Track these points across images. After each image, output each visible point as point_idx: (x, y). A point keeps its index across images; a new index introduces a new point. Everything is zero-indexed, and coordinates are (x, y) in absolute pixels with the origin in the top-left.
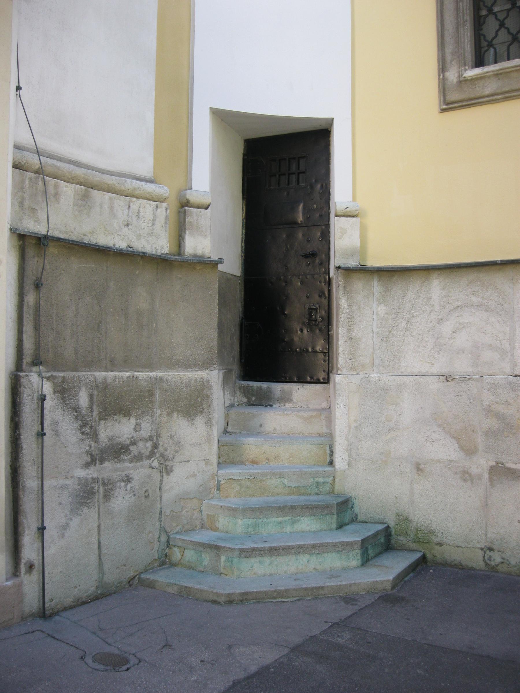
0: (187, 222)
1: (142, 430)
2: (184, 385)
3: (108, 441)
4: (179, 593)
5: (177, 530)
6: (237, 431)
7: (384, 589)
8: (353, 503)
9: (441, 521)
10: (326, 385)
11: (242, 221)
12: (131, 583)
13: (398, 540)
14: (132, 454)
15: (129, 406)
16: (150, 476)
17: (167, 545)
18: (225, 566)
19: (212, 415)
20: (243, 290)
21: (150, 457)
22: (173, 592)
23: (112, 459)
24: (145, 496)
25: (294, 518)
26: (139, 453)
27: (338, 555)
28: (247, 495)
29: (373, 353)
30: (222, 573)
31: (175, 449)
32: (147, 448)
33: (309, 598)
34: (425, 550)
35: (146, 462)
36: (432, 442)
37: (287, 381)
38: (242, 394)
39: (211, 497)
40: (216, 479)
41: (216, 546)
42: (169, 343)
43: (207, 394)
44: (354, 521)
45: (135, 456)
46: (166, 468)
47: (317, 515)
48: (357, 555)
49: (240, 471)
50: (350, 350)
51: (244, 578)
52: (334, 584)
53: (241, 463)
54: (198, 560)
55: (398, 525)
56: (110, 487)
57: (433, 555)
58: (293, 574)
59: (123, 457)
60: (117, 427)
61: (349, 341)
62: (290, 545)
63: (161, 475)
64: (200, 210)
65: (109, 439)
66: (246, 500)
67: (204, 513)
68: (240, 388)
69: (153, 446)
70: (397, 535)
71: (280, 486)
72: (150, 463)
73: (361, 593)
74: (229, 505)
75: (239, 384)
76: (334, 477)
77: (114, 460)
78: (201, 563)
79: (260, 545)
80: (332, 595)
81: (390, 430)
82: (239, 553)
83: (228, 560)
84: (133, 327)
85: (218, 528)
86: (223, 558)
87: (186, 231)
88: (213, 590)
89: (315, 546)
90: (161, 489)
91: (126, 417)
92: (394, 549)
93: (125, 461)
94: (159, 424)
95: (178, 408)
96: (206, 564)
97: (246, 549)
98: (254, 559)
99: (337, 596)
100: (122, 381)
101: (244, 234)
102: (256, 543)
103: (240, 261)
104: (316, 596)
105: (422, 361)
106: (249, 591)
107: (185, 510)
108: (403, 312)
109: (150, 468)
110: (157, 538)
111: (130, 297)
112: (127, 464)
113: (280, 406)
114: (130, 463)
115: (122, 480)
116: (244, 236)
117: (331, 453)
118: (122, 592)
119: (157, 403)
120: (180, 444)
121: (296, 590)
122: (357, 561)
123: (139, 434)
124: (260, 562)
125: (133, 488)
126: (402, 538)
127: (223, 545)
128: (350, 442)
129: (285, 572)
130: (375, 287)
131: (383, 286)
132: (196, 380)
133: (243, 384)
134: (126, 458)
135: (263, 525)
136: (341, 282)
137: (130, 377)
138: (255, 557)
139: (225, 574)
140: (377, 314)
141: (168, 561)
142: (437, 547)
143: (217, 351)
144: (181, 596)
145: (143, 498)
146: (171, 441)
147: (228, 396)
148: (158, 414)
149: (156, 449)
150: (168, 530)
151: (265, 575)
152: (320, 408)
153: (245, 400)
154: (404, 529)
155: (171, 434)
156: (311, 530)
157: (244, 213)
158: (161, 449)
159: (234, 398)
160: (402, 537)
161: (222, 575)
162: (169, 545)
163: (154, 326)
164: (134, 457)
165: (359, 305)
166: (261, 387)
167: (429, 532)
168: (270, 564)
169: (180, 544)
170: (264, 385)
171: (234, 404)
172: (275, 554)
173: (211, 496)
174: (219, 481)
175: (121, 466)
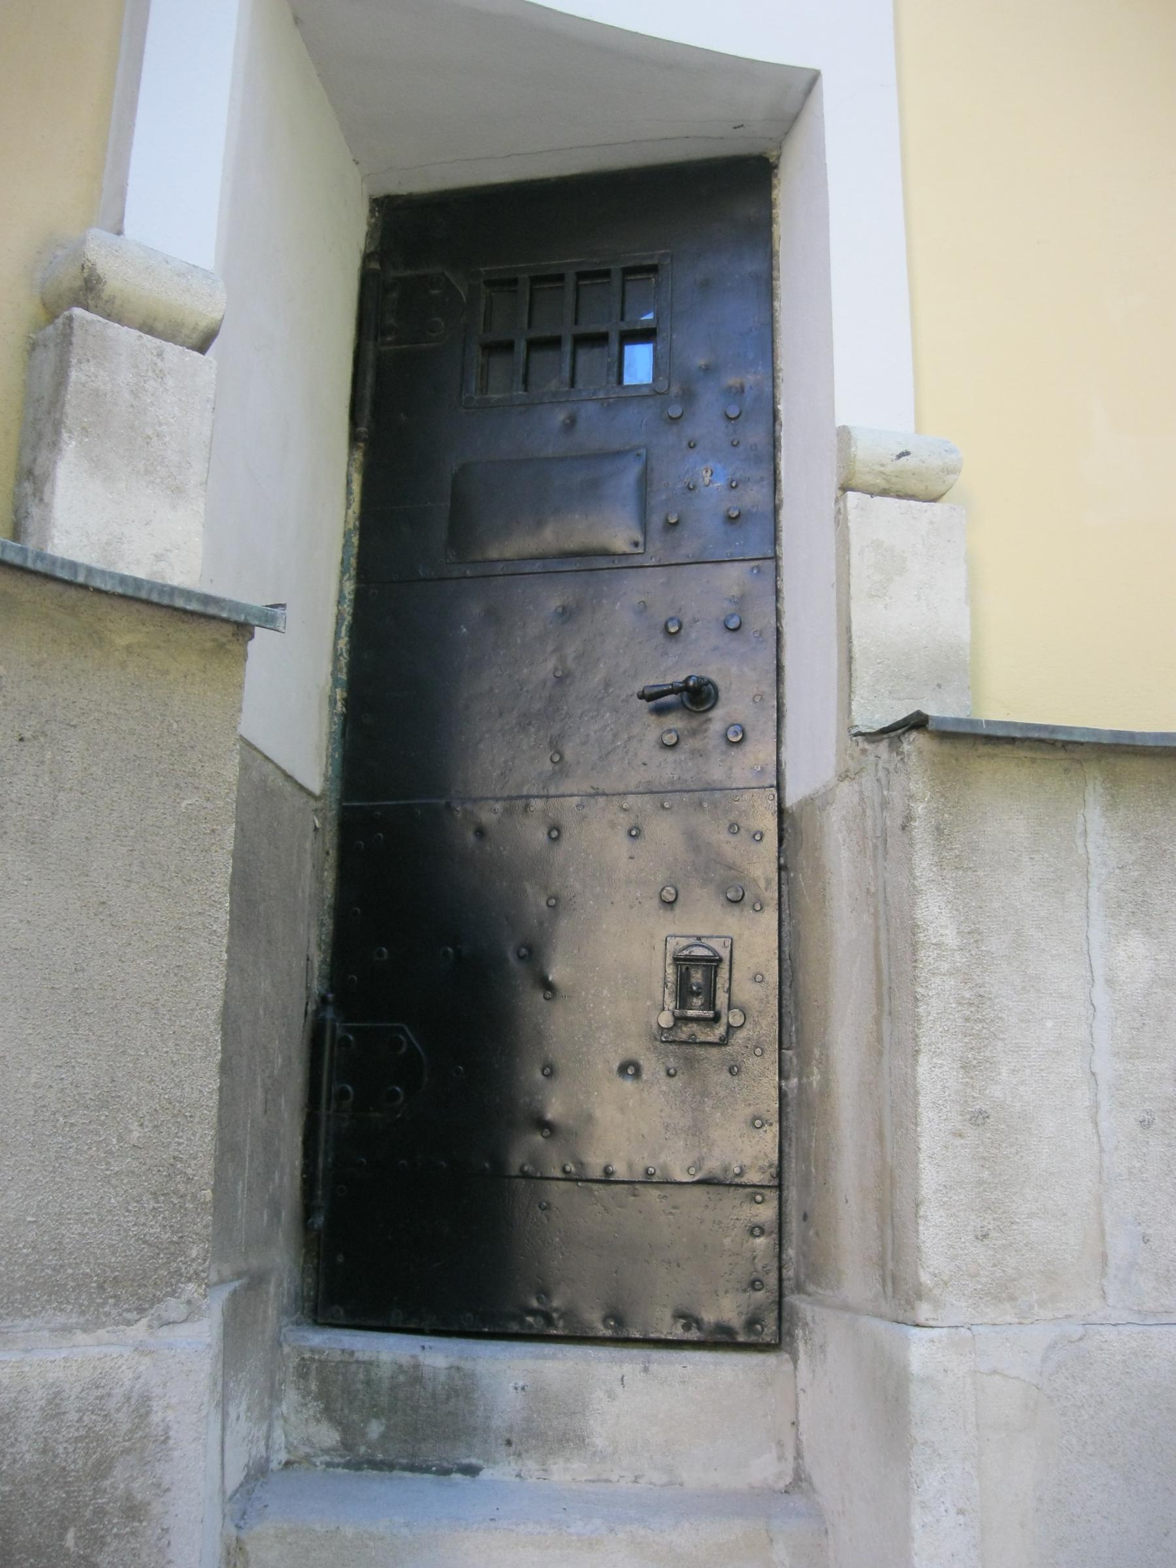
0: (71, 388)
11: (340, 541)
38: (315, 1407)
43: (129, 1496)
50: (981, 1182)
64: (158, 342)
68: (303, 1372)
87: (65, 435)
101: (349, 596)
103: (326, 722)
113: (519, 1475)
116: (347, 608)
133: (321, 1352)
136: (922, 800)
140: (1110, 982)
143: (214, 1191)
147: (241, 1427)
153: (328, 1436)
157: (356, 506)
166: (417, 1366)
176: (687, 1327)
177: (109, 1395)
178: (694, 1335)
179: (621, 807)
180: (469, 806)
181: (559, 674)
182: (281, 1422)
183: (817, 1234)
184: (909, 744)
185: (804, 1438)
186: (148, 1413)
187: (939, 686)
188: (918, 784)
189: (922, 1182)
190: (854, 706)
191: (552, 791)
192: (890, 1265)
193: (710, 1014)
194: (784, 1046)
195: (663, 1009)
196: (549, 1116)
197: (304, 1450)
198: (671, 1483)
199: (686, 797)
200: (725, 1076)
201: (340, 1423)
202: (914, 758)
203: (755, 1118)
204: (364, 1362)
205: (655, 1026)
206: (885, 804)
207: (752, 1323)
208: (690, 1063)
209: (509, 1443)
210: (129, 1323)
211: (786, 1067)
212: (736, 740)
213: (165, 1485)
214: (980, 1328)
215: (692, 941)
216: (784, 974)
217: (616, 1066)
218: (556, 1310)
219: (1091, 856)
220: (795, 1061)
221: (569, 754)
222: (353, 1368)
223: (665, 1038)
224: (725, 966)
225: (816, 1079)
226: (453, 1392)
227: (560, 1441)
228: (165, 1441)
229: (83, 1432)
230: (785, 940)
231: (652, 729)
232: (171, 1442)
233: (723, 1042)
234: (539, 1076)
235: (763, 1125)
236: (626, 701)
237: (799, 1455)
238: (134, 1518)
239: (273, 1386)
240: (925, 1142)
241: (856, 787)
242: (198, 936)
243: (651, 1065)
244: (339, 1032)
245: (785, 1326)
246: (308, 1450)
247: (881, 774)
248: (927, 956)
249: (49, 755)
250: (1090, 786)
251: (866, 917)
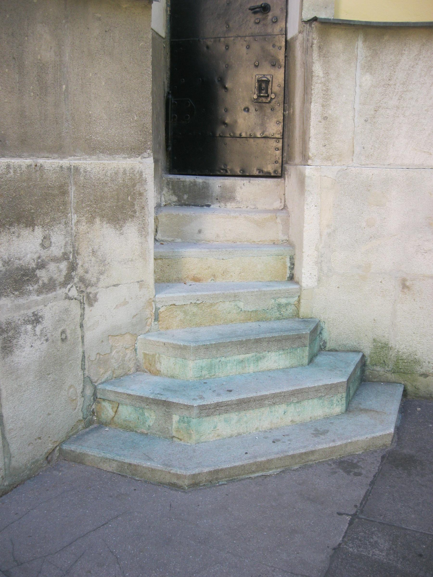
1: (53, 245)
2: (109, 179)
3: (4, 266)
4: (119, 472)
5: (106, 377)
6: (170, 239)
7: (384, 445)
8: (321, 328)
9: (428, 349)
10: (279, 180)
12: (49, 458)
13: (373, 370)
14: (41, 282)
15: (32, 211)
16: (67, 310)
17: (94, 399)
18: (178, 428)
19: (146, 221)
20: (168, 56)
21: (66, 284)
22: (110, 470)
23: (12, 293)
24: (62, 339)
25: (258, 355)
26: (51, 279)
27: (321, 401)
28: (193, 325)
29: (353, 139)
30: (174, 437)
31: (98, 270)
32: (61, 271)
33: (296, 467)
34: (405, 382)
35: (61, 292)
36: (424, 254)
37: (228, 174)
38: (171, 192)
39: (147, 330)
40: (154, 306)
41: (165, 401)
42: (86, 116)
43: (140, 191)
44: (322, 350)
45: (44, 284)
46: (88, 297)
47: (287, 348)
48: (342, 400)
49: (184, 294)
50: (325, 133)
51: (205, 442)
52: (327, 446)
53: (179, 280)
54: (138, 419)
55: (374, 353)
56: (10, 334)
57: (415, 388)
58: (266, 432)
59: (27, 287)
60: (16, 243)
61: (323, 121)
62: (263, 395)
63: (82, 307)
65: (5, 262)
66: (195, 332)
67: (140, 353)
68: (168, 184)
69: (68, 268)
70: (373, 365)
71: (235, 311)
72: (67, 291)
73: (357, 453)
74: (175, 342)
75: (167, 179)
76: (299, 296)
77: (13, 294)
78: (144, 423)
79: (225, 398)
80: (323, 460)
81: (371, 237)
82: (198, 411)
83: (182, 421)
84: (32, 88)
85: (160, 371)
86: (176, 418)
88: (171, 470)
89: (293, 393)
90: (83, 327)
91: (28, 228)
92: (369, 381)
93: (31, 293)
94: (76, 235)
95: (101, 211)
96: (151, 424)
97: (207, 405)
98: (217, 417)
99: (330, 460)
100: (19, 172)
102: (219, 395)
104: (304, 463)
105: (416, 150)
106: (220, 468)
107: (115, 351)
108: (395, 85)
109: (67, 299)
110: (80, 393)
111: (26, 38)
112: (34, 297)
113: (219, 207)
114: (38, 296)
115: (27, 322)
117: (292, 266)
118: (38, 475)
119: (72, 205)
120: (106, 262)
121: (281, 459)
122: (342, 407)
123: (49, 252)
124: (226, 421)
125: (45, 330)
126: (378, 368)
127: (175, 400)
128: (321, 253)
129: (257, 429)
130: (359, 49)
131: (370, 48)
132: (125, 171)
133: (172, 179)
134: (31, 288)
135: (221, 367)
137: (31, 165)
138: (219, 415)
139: (178, 438)
140: (360, 86)
141: (95, 418)
142: (421, 379)
144: (123, 476)
145: (59, 343)
146: (93, 259)
148: (74, 221)
149: (73, 271)
150: (94, 379)
151: (231, 437)
152: (271, 208)
153: (175, 198)
154: (381, 357)
155: (93, 249)
156: (278, 368)
158: (80, 271)
159: (161, 196)
160: (379, 367)
161: (175, 439)
162: (97, 398)
163: (64, 90)
164: (44, 286)
165: (338, 74)
166: (195, 182)
167: (412, 361)
168: (239, 421)
169: (112, 397)
170: (200, 180)
171: (161, 204)
172: (245, 408)
173: (148, 328)
174: (157, 309)
175: (25, 302)
176: (259, 172)
177: (135, 171)
178: (261, 174)
179: (244, 40)
180: (204, 40)
181: (228, 2)
182: (163, 196)
183: (291, 149)
184: (313, 25)
185: (286, 197)
186: (142, 175)
187: (326, 8)
188: (315, 35)
189: (311, 133)
190: (303, 13)
191: (226, 36)
192: (304, 153)
193: (267, 95)
194: (285, 103)
195: (255, 94)
196: (226, 122)
197: (169, 202)
198: (255, 208)
199: (261, 37)
200: (270, 111)
201: (177, 195)
202: (314, 29)
203: (277, 121)
204: (182, 181)
205: (253, 98)
206: (308, 40)
207: (275, 172)
208: (261, 108)
209: (217, 199)
210: (137, 157)
211: (285, 109)
212: (275, 21)
213: (146, 190)
214: (323, 166)
215: (262, 76)
216: (286, 85)
217: (243, 108)
218: (228, 169)
219: (358, 54)
220: (287, 107)
221: (230, 25)
222: (180, 182)
223: (256, 101)
224: (271, 83)
225: (292, 111)
226: (204, 188)
227: (229, 199)
228: (146, 181)
229: (130, 178)
230: (286, 76)
231: (252, 18)
232: (147, 181)
233: (270, 102)
234: (223, 111)
235: (279, 123)
236: (246, 10)
237: (285, 201)
238: (141, 196)
239: (161, 186)
240: (312, 124)
241: (302, 35)
242: (145, 75)
243: (252, 109)
244: (173, 102)
245: (283, 172)
246: (170, 202)
247: (307, 32)
248: (315, 79)
249: (112, 35)
250: (360, 36)
251: (303, 69)
